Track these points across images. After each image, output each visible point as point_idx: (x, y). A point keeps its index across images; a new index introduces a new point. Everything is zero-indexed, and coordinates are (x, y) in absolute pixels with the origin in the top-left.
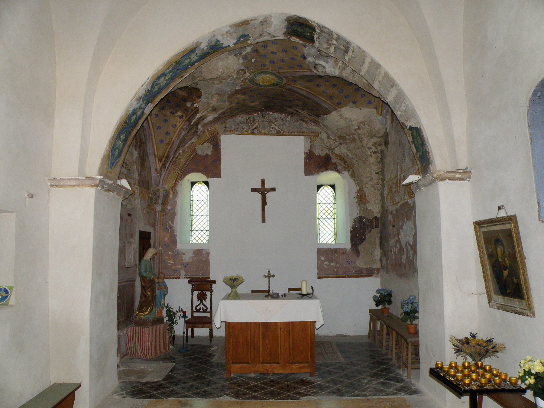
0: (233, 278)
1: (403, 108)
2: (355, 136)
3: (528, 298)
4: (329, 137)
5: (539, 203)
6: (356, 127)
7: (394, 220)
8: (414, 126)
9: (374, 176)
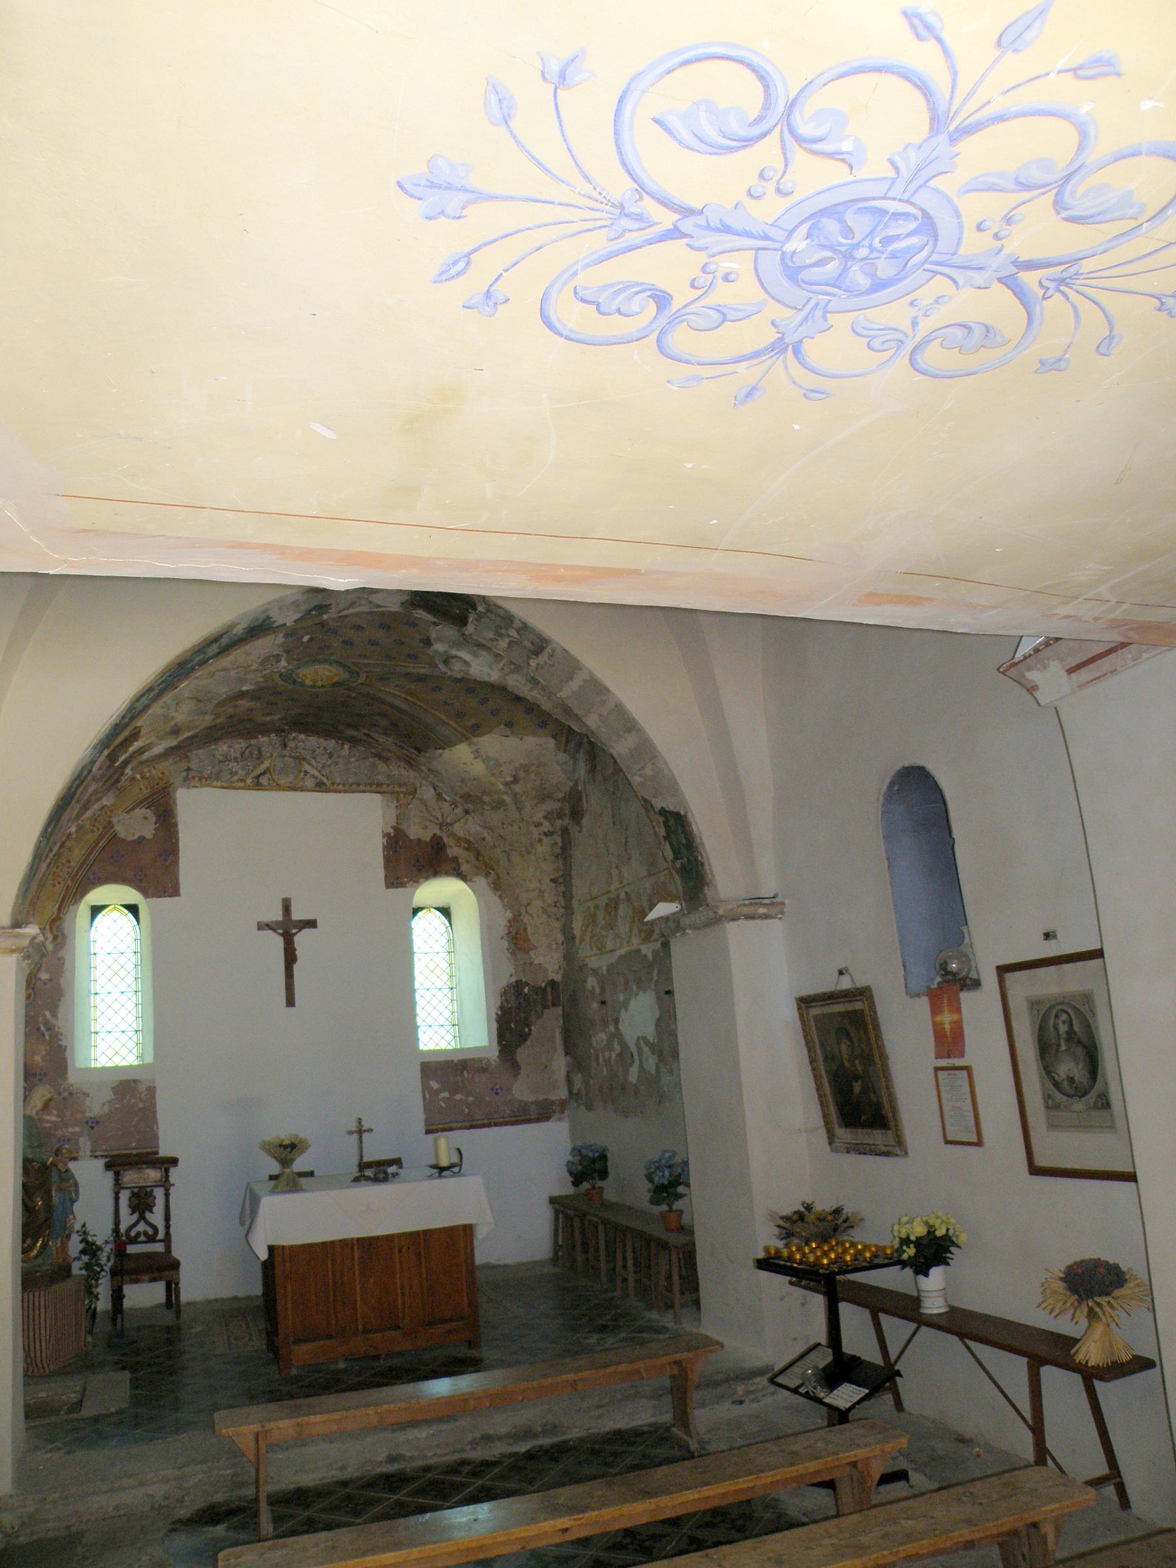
0: (286, 1142)
1: (649, 772)
2: (505, 797)
3: (896, 1126)
4: (439, 796)
5: (904, 966)
6: (509, 779)
7: (603, 990)
8: (672, 808)
9: (546, 885)
